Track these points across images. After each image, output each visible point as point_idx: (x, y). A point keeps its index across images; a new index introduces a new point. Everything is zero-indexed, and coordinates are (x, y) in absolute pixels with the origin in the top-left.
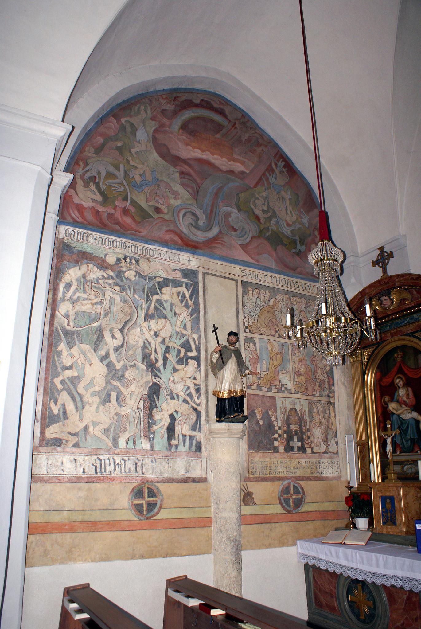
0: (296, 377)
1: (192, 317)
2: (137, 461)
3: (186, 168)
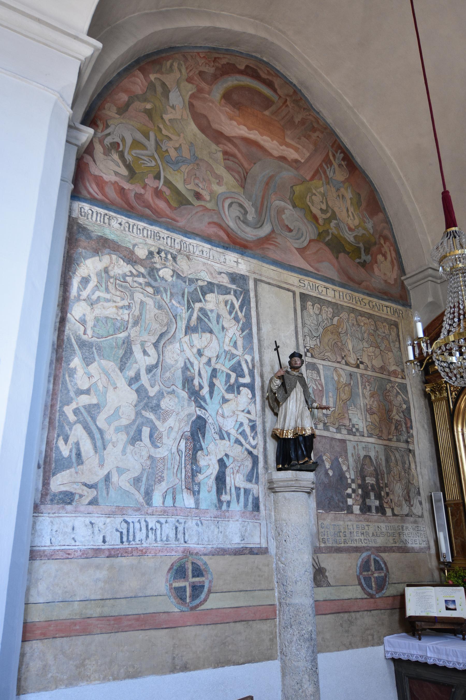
0: (368, 416)
1: (244, 333)
2: (177, 524)
3: (230, 148)
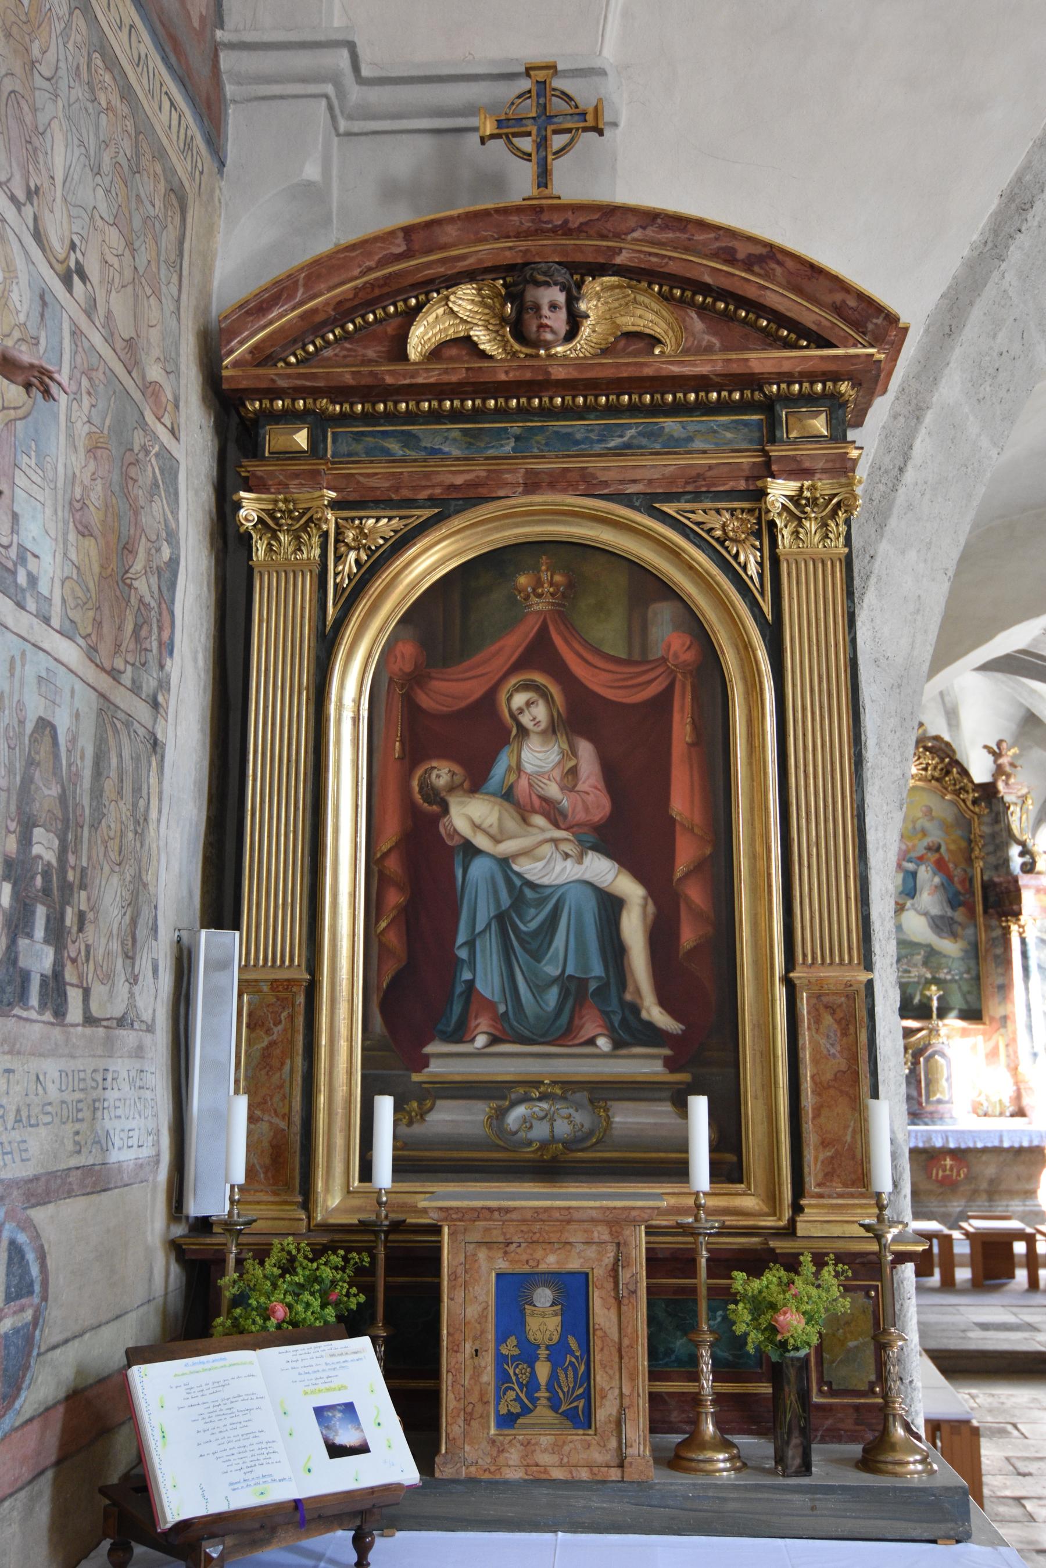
0: (72, 536)
